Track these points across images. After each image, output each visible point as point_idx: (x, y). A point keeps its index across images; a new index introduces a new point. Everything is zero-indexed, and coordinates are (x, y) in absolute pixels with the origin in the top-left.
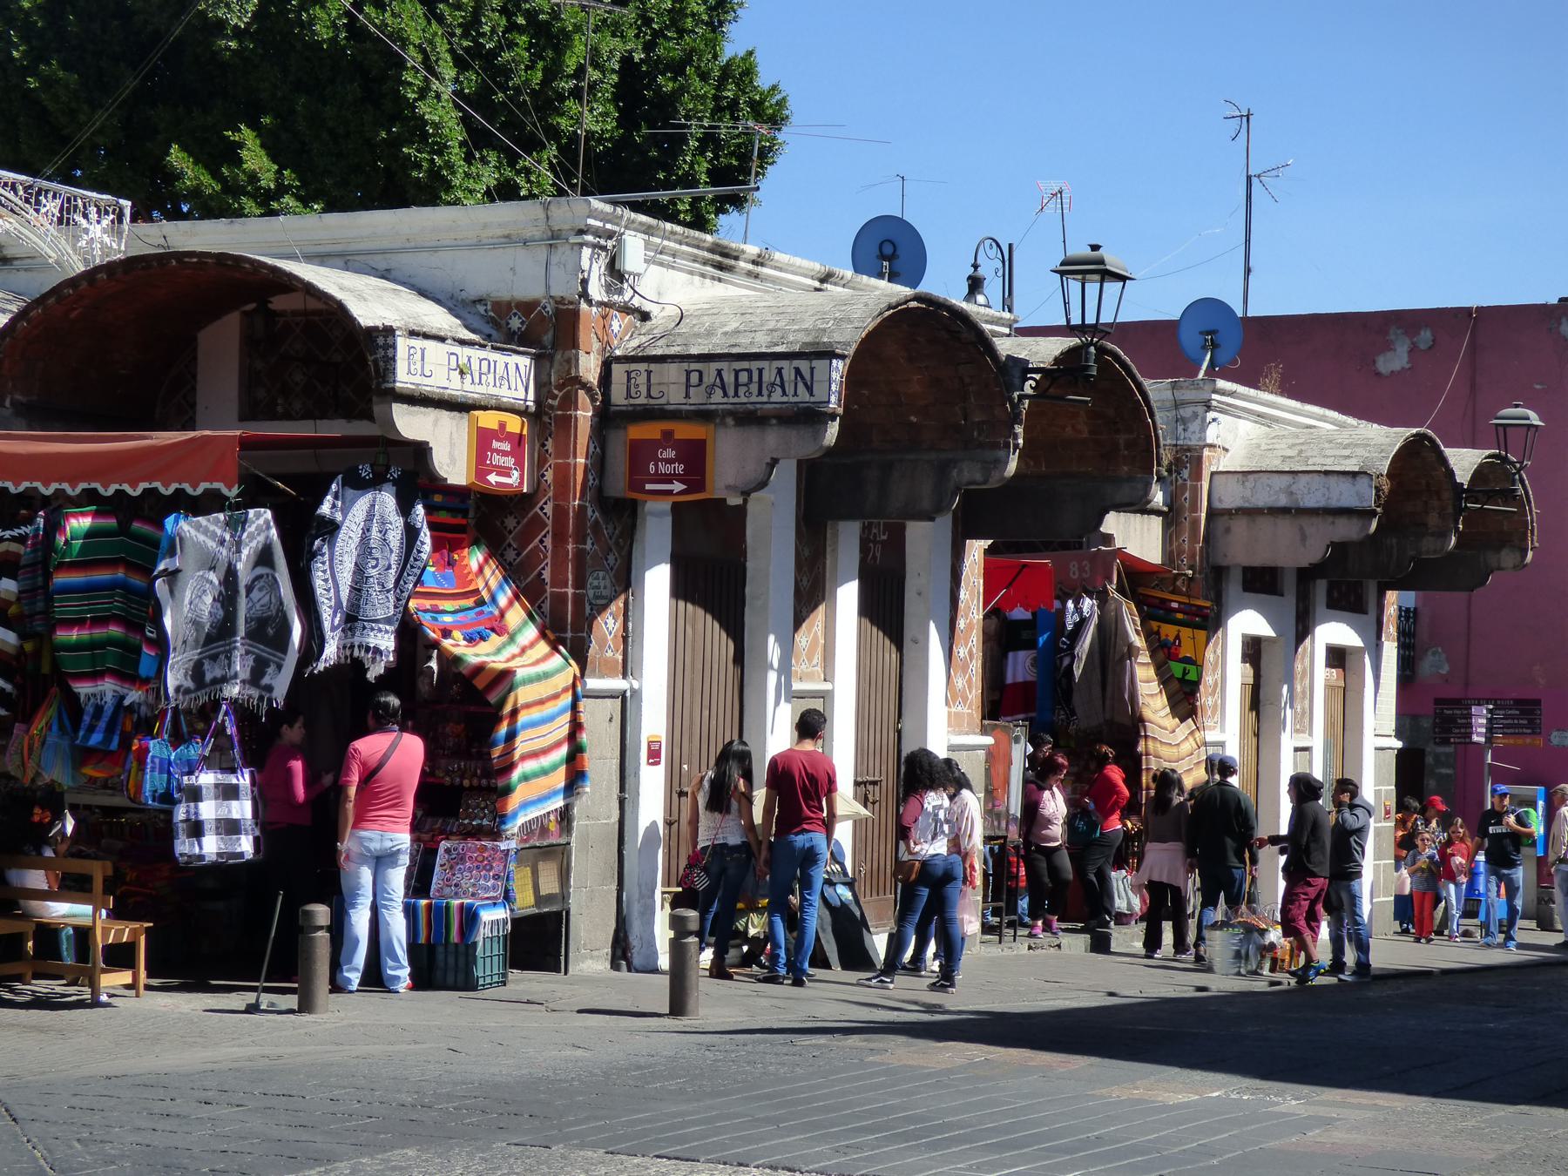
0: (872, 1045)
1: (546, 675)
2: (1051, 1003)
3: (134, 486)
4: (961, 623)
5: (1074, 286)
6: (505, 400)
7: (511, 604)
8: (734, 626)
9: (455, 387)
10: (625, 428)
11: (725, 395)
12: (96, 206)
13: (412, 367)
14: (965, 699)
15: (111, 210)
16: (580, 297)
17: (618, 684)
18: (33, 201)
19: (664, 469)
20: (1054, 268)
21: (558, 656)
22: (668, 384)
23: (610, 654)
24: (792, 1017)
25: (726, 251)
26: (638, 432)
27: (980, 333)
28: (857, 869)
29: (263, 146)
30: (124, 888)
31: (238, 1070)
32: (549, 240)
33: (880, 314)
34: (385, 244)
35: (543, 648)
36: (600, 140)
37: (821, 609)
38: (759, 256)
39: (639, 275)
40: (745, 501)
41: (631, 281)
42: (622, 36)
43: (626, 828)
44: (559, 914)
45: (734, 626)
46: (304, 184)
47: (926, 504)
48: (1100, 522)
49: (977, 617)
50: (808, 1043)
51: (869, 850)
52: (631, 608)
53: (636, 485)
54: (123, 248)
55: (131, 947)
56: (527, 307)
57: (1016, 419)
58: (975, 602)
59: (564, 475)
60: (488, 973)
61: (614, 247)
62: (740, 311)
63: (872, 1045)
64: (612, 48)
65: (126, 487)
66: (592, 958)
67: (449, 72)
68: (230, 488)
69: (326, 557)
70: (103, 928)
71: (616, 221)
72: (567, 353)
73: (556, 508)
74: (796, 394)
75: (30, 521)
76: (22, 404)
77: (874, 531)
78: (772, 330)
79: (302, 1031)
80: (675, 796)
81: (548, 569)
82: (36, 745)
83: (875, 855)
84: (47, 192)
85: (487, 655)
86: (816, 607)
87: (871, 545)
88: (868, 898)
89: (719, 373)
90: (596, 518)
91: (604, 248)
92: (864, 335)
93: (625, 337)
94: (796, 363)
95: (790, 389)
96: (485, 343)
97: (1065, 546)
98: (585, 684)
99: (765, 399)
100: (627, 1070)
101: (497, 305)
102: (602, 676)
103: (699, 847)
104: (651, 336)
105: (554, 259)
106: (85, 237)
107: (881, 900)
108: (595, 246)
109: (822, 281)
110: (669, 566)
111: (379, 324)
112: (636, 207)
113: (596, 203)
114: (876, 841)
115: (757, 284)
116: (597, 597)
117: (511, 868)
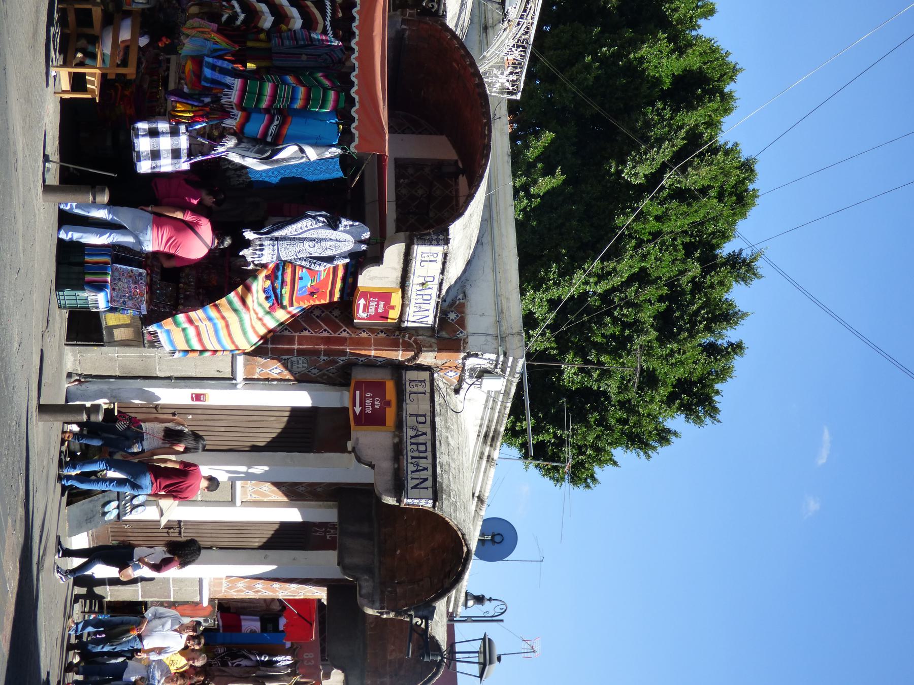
0: (18, 522)
1: (244, 333)
2: (43, 639)
3: (357, 92)
4: (276, 585)
5: (477, 646)
6: (408, 309)
7: (289, 313)
8: (274, 446)
9: (415, 280)
10: (392, 379)
11: (412, 437)
12: (517, 79)
13: (426, 255)
14: (230, 588)
15: (515, 88)
16: (468, 353)
17: (240, 375)
18: (519, 44)
19: (368, 402)
20: (487, 634)
21: (258, 339)
22: (418, 404)
23: (258, 370)
24: (37, 477)
25: (495, 439)
26: (390, 386)
27: (449, 590)
28: (128, 523)
29: (553, 188)
30: (120, 88)
31: (8, 143)
32: (500, 335)
33: (459, 529)
34: (497, 242)
35: (262, 331)
36: (559, 379)
37: (285, 499)
38: (493, 459)
39: (480, 387)
40: (350, 452)
41: (477, 383)
42: (619, 393)
43: (153, 381)
44: (101, 340)
45: (274, 446)
46: (533, 210)
47: (348, 561)
48: (338, 668)
49: (280, 595)
50: (20, 483)
51: (139, 530)
52: (286, 383)
53: (359, 385)
54: (493, 94)
55: (84, 90)
56: (462, 323)
57: (398, 613)
58: (289, 594)
59: (364, 343)
60: (66, 298)
61: (497, 373)
62: (460, 447)
63: (18, 522)
64: (611, 386)
65: (356, 88)
66: (75, 361)
67: (600, 289)
68: (356, 147)
69: (316, 226)
70: (96, 73)
71: (512, 374)
72: (435, 345)
73: (345, 339)
74: (412, 479)
75: (336, 36)
76: (403, 35)
77: (332, 531)
78: (449, 465)
79: (32, 186)
80: (173, 411)
81: (309, 334)
82: (205, 35)
83: (136, 534)
84: (525, 52)
85: (257, 298)
86: (286, 495)
87: (324, 529)
88: (110, 530)
89: (425, 434)
90: (339, 362)
91: (496, 366)
92: (447, 519)
93: (445, 380)
94: (430, 479)
95: (416, 475)
96: (441, 298)
97: (323, 651)
98: (239, 355)
99: (409, 460)
100: (5, 372)
101: (462, 306)
102: (245, 365)
103: (142, 424)
104: (445, 395)
105: (489, 338)
106: (499, 73)
107: (109, 538)
108: (497, 361)
109: (479, 497)
110: (310, 406)
111: (450, 237)
112: (520, 386)
113: (522, 362)
114: (145, 534)
115: (477, 458)
116: (292, 363)
117: (129, 312)
